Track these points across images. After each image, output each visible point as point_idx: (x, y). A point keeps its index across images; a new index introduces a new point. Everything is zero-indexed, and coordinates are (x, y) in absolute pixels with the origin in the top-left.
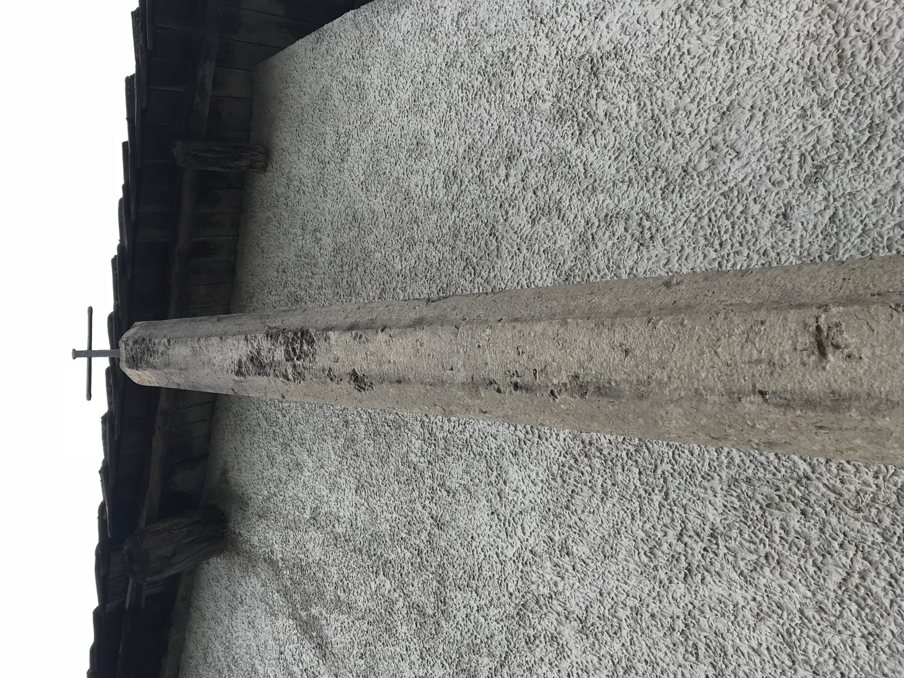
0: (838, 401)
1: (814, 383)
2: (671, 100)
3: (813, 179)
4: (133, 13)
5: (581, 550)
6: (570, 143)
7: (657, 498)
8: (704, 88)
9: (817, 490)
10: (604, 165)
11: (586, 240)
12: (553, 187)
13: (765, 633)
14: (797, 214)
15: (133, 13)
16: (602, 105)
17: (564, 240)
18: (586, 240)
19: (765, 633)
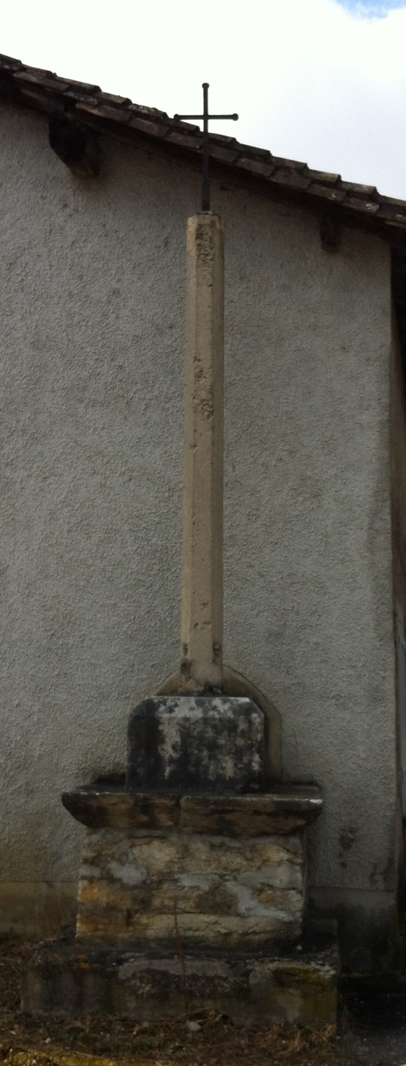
3: (261, 575)
7: (157, 519)
14: (250, 570)
16: (300, 499)
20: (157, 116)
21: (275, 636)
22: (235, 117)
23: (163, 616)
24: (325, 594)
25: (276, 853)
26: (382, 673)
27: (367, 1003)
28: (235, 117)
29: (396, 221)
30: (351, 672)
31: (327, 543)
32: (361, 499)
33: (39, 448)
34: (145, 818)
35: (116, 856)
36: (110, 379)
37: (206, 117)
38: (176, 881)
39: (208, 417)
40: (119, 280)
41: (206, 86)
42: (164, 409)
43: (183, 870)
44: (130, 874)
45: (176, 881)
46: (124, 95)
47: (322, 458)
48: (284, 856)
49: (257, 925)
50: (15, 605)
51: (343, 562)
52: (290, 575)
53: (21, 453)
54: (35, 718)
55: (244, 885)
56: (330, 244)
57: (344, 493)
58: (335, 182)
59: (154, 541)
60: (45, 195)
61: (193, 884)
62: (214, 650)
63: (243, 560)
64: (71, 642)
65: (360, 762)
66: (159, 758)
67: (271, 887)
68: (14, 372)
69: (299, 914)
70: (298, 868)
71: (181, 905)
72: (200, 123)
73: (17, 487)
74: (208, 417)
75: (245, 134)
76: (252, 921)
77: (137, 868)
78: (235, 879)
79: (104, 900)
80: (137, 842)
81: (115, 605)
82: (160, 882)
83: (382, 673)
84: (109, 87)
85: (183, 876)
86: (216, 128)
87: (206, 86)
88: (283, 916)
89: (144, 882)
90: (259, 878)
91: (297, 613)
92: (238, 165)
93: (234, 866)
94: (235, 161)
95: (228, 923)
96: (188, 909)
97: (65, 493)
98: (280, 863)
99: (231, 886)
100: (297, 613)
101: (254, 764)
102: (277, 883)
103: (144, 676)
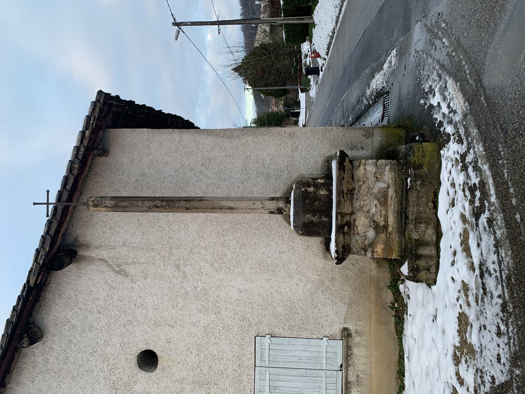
0: (255, 209)
1: (253, 207)
2: (223, 168)
3: (242, 183)
4: (239, 69)
5: (205, 236)
6: (205, 171)
7: (219, 226)
8: (228, 168)
9: (242, 222)
10: (212, 176)
11: (208, 186)
12: (201, 177)
13: (235, 242)
14: (240, 187)
15: (239, 69)
16: (211, 166)
17: (203, 186)
18: (208, 186)
19: (235, 242)
20: (50, 223)
21: (268, 177)
22: (48, 191)
23: (259, 223)
24: (250, 156)
25: (360, 172)
26: (283, 132)
27: (365, 211)
28: (48, 191)
29: (93, 123)
30: (282, 146)
31: (229, 155)
32: (211, 141)
33: (189, 276)
34: (346, 227)
35: (363, 241)
36: (160, 246)
37: (48, 204)
38: (373, 214)
39: (174, 202)
40: (119, 242)
41: (35, 204)
42: (173, 223)
43: (368, 212)
44: (371, 234)
45: (373, 214)
46: (40, 238)
47: (194, 157)
48: (362, 167)
49: (392, 179)
50: (255, 286)
51: (237, 149)
52: (242, 171)
53: (191, 284)
54: (302, 277)
55: (374, 186)
56: (105, 152)
57: (208, 148)
58: (77, 149)
59: (228, 227)
60: (83, 273)
61: (374, 207)
62: (273, 200)
63: (236, 190)
64: (270, 262)
65: (319, 141)
66: (319, 223)
67: (375, 173)
68: (157, 286)
69: (387, 161)
70: (367, 162)
71: (384, 212)
72: (51, 207)
73: (204, 285)
74: (174, 202)
75: (56, 187)
76: (390, 181)
77: (369, 232)
78: (372, 189)
79: (382, 246)
80: (356, 232)
81: (255, 243)
82: (374, 221)
83: (283, 132)
84: (37, 245)
85: (371, 212)
86: (53, 199)
87: (35, 204)
88: (387, 168)
89: (374, 229)
90: (372, 179)
91: (258, 168)
92: (69, 189)
93: (366, 190)
94: (68, 191)
95: (391, 192)
96: (385, 209)
97: (208, 265)
98: (365, 169)
99: (375, 190)
100: (258, 168)
101: (322, 182)
102: (374, 170)
103: (284, 232)
